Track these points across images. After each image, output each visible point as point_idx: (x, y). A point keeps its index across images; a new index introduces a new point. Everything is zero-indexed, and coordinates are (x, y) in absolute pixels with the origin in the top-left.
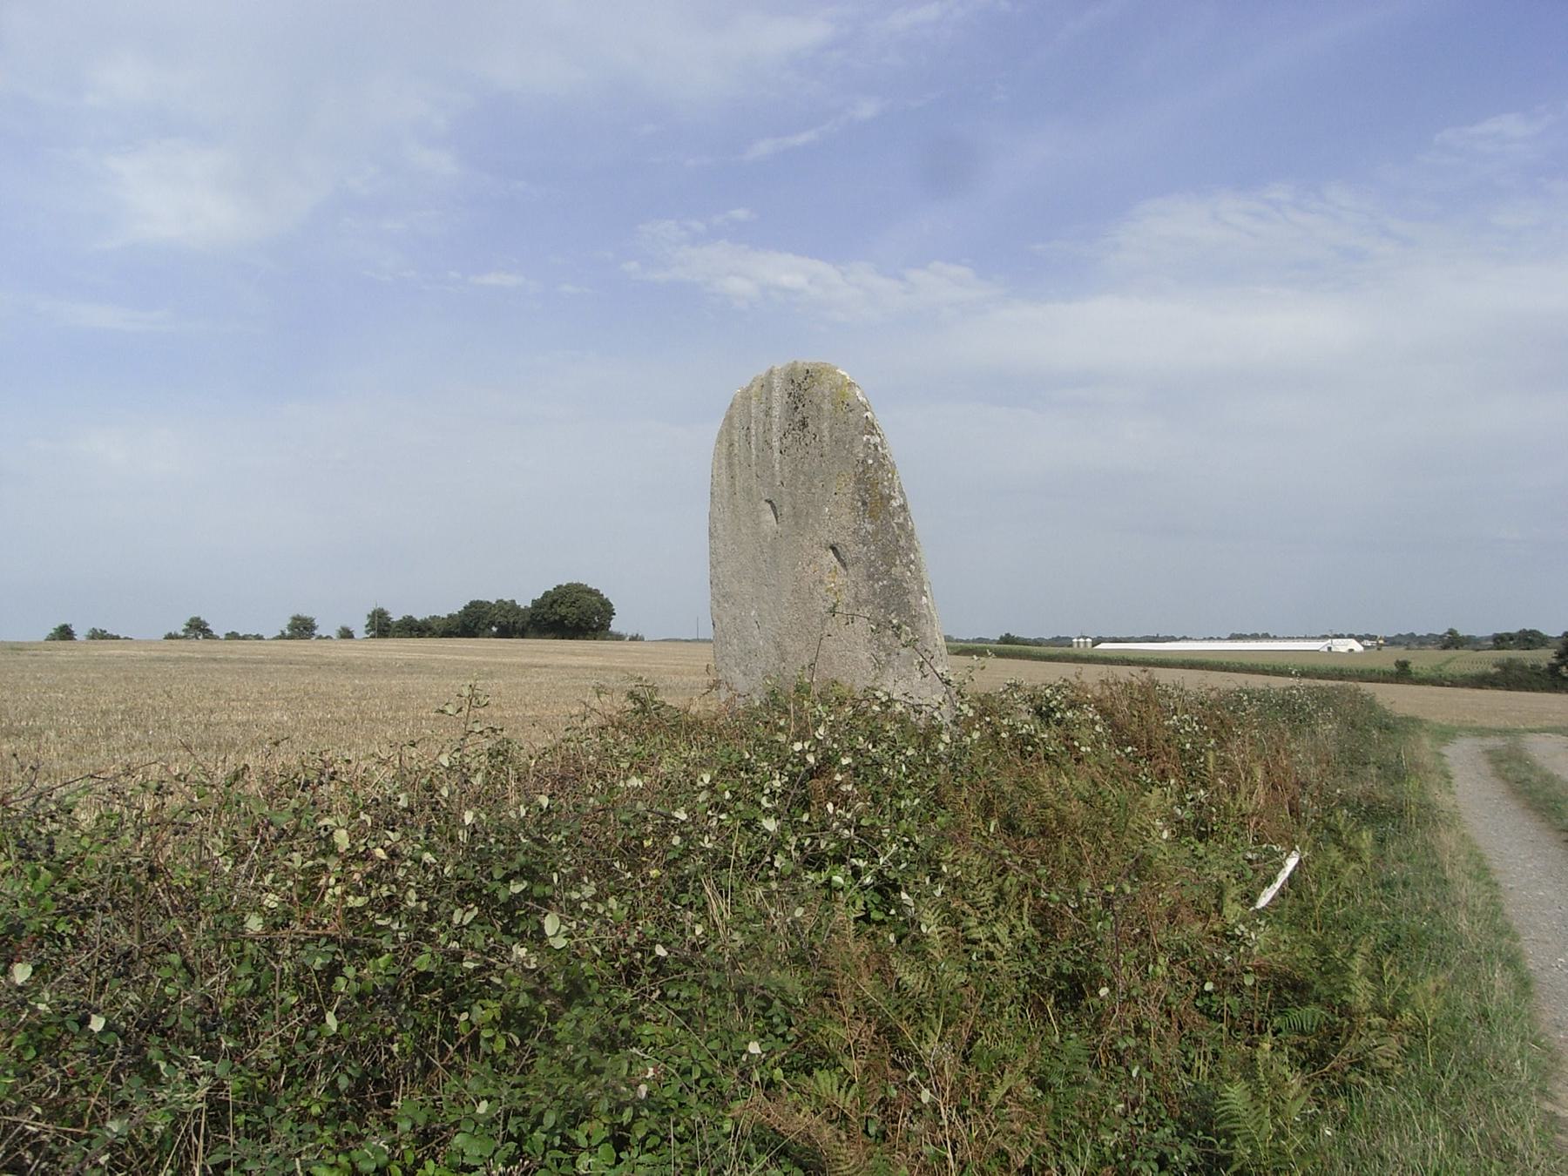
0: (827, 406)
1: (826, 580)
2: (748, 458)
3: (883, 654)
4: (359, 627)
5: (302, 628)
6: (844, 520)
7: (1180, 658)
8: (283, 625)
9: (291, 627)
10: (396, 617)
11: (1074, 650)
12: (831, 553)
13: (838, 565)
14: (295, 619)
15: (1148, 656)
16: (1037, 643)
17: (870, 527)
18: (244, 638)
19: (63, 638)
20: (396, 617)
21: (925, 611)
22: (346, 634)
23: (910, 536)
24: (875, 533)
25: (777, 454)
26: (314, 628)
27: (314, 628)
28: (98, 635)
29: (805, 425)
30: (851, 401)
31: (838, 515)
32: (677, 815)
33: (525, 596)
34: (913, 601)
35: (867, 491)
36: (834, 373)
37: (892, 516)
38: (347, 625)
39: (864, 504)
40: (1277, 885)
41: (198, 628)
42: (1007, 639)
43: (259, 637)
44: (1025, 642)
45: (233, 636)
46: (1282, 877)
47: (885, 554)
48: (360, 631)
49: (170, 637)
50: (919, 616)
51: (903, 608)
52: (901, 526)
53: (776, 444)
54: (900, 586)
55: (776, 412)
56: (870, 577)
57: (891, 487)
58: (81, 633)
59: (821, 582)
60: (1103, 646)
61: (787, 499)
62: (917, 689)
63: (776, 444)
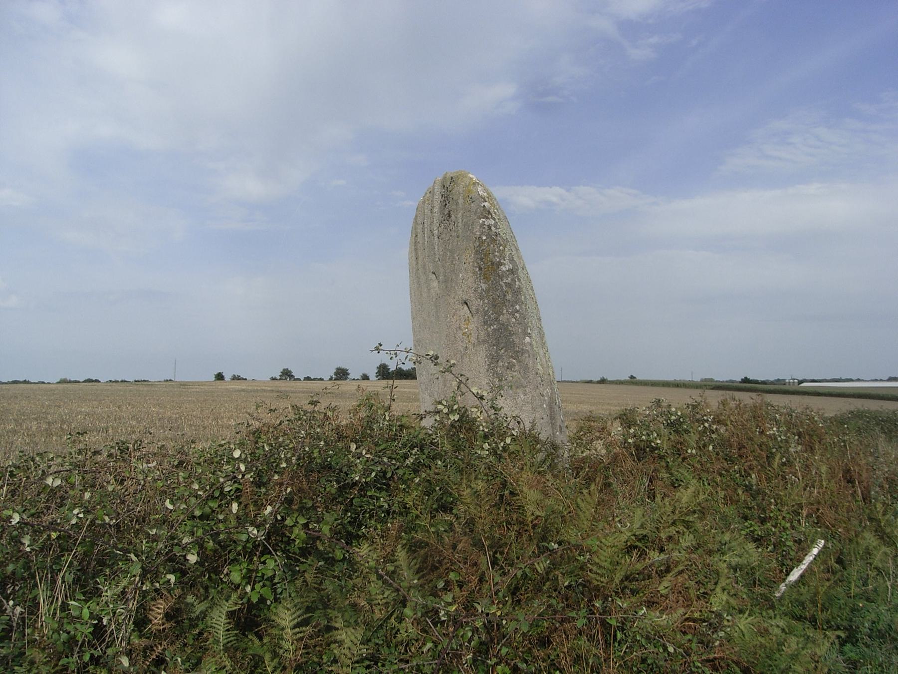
0: (461, 201)
1: (463, 326)
2: (424, 243)
3: (496, 380)
4: (372, 374)
5: (342, 374)
6: (471, 280)
7: (852, 392)
8: (332, 372)
9: (336, 374)
10: (392, 368)
11: (786, 387)
12: (466, 308)
13: (470, 316)
14: (338, 369)
15: (845, 391)
16: (764, 383)
17: (484, 286)
18: (314, 379)
19: (218, 379)
20: (392, 368)
21: (528, 348)
22: (365, 377)
23: (518, 292)
24: (488, 291)
25: (436, 239)
26: (348, 374)
27: (348, 374)
28: (236, 378)
29: (450, 216)
30: (473, 195)
31: (467, 281)
32: (234, 511)
33: (697, 379)
34: (517, 341)
35: (481, 259)
36: (466, 177)
37: (501, 278)
38: (366, 373)
39: (480, 269)
40: (803, 567)
41: (287, 374)
42: (746, 380)
43: (321, 379)
44: (756, 382)
45: (308, 379)
46: (809, 559)
47: (494, 306)
48: (373, 375)
49: (273, 379)
50: (523, 352)
51: (510, 346)
52: (508, 285)
53: (436, 232)
54: (506, 329)
55: (436, 210)
56: (485, 323)
57: (502, 256)
58: (228, 377)
59: (460, 328)
60: (805, 384)
61: (442, 270)
62: (520, 409)
63: (436, 232)
